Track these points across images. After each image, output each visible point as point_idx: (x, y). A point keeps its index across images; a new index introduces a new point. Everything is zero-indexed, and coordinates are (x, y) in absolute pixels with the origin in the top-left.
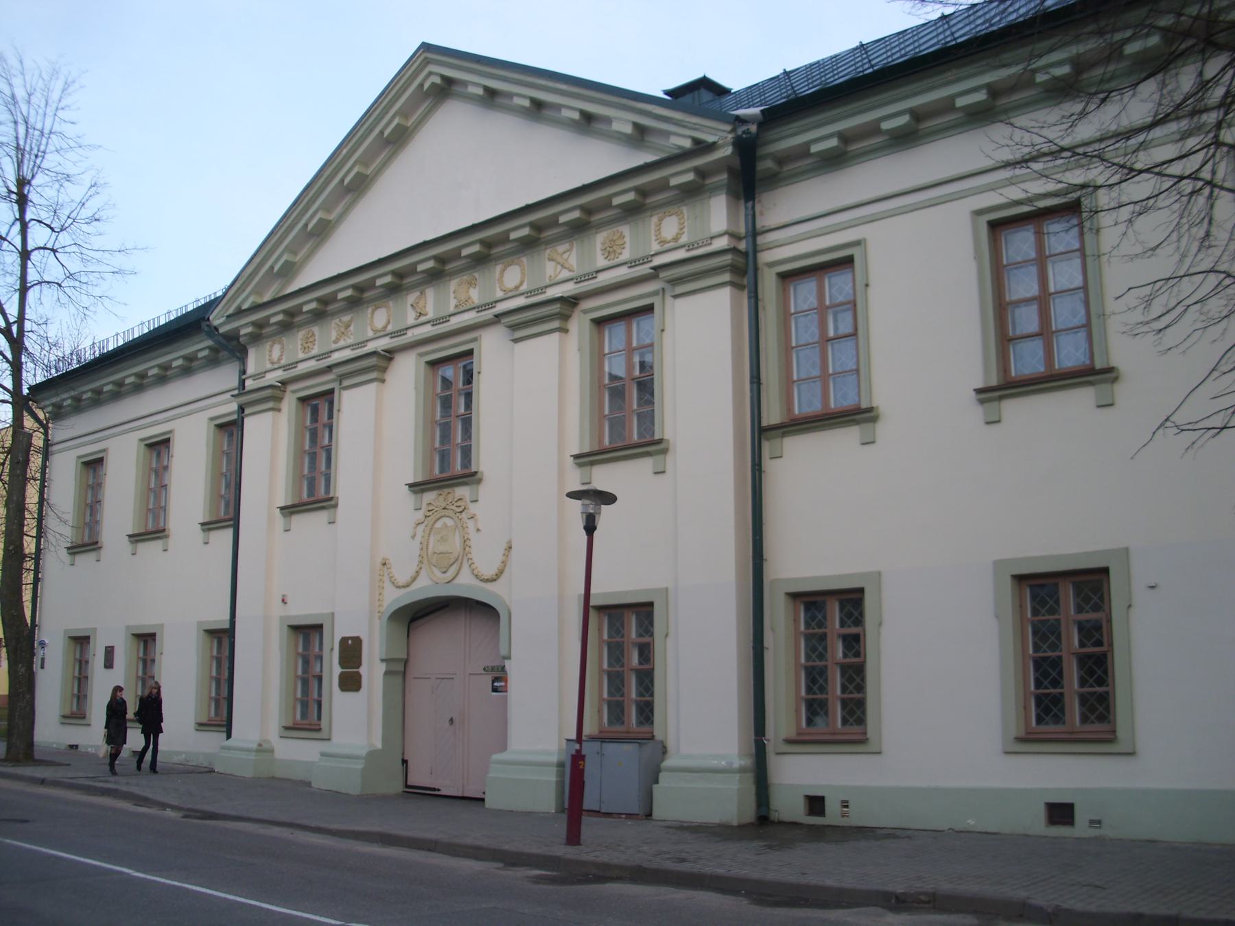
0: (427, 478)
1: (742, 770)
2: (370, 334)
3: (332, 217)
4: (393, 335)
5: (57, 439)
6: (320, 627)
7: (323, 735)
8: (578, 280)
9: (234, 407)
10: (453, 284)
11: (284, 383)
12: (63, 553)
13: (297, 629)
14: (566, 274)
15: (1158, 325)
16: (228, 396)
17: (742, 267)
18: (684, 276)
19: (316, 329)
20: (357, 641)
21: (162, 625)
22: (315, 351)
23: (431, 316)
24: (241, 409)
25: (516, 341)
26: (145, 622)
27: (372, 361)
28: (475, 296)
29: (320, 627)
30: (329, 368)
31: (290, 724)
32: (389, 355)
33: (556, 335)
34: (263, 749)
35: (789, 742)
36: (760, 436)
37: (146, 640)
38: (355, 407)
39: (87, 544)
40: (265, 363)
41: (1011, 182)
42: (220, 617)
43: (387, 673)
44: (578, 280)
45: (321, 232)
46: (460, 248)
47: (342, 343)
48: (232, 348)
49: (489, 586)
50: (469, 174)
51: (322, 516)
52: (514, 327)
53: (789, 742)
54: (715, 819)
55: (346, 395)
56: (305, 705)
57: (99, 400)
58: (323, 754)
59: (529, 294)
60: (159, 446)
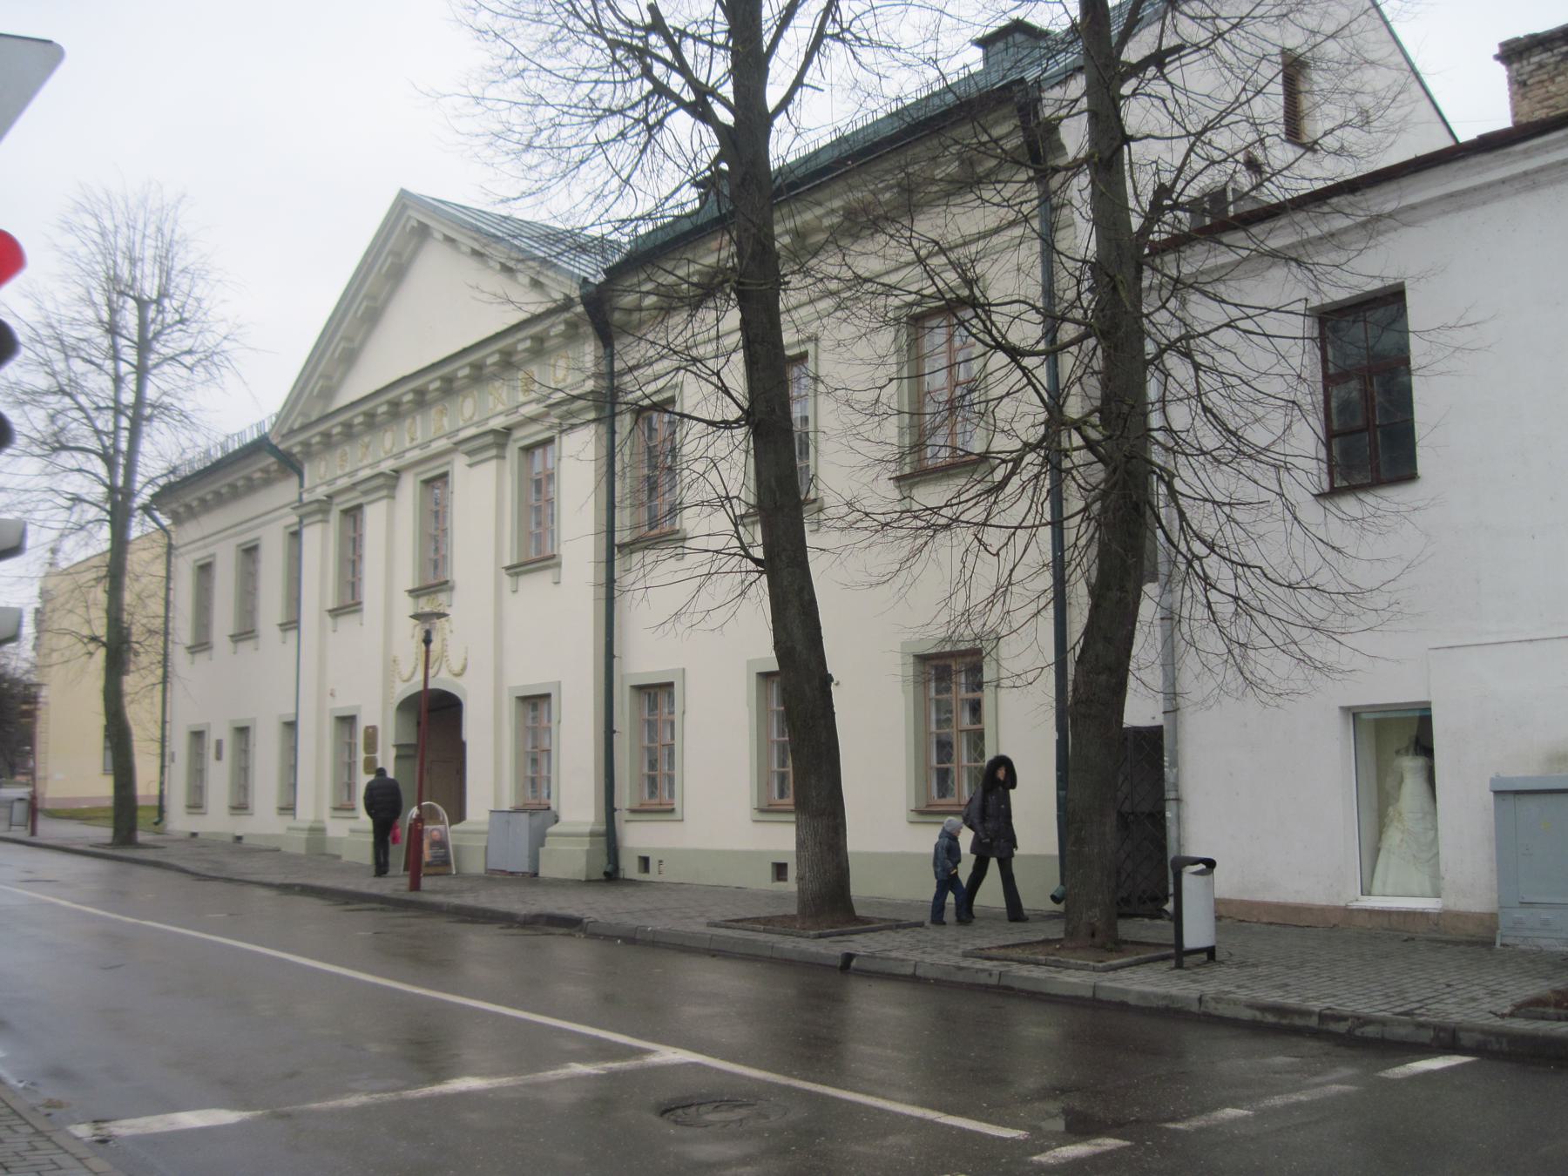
0: (423, 584)
1: (592, 834)
2: (382, 455)
3: (356, 344)
4: (478, 424)
5: (181, 542)
6: (671, 685)
7: (678, 816)
8: (507, 413)
9: (295, 519)
10: (433, 412)
11: (330, 497)
12: (277, 631)
13: (524, 699)
14: (500, 408)
15: (224, 619)
16: (288, 510)
17: (606, 402)
18: (564, 412)
19: (347, 448)
20: (374, 728)
21: (209, 725)
22: (348, 470)
23: (419, 441)
24: (301, 522)
25: (470, 466)
26: (242, 718)
27: (381, 481)
28: (447, 425)
29: (671, 685)
30: (355, 485)
31: (636, 807)
32: (397, 473)
33: (493, 463)
34: (317, 831)
35: (633, 811)
36: (612, 551)
37: (243, 732)
38: (374, 516)
39: (201, 645)
40: (321, 476)
41: (199, 549)
42: (288, 712)
43: (398, 757)
44: (507, 413)
45: (349, 358)
46: (516, 344)
47: (365, 462)
48: (290, 465)
49: (458, 680)
50: (451, 310)
51: (545, 578)
52: (469, 453)
53: (633, 811)
54: (569, 876)
55: (565, 438)
56: (653, 781)
57: (236, 494)
58: (352, 831)
59: (478, 424)
60: (250, 552)
